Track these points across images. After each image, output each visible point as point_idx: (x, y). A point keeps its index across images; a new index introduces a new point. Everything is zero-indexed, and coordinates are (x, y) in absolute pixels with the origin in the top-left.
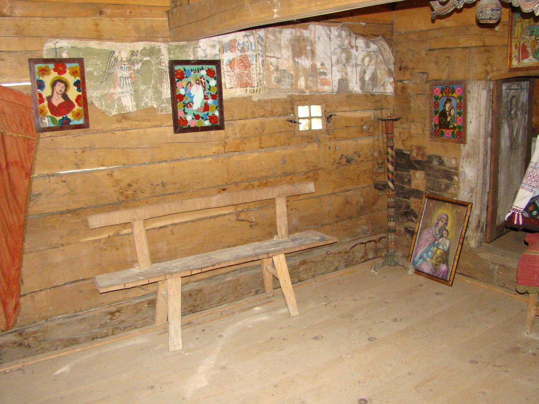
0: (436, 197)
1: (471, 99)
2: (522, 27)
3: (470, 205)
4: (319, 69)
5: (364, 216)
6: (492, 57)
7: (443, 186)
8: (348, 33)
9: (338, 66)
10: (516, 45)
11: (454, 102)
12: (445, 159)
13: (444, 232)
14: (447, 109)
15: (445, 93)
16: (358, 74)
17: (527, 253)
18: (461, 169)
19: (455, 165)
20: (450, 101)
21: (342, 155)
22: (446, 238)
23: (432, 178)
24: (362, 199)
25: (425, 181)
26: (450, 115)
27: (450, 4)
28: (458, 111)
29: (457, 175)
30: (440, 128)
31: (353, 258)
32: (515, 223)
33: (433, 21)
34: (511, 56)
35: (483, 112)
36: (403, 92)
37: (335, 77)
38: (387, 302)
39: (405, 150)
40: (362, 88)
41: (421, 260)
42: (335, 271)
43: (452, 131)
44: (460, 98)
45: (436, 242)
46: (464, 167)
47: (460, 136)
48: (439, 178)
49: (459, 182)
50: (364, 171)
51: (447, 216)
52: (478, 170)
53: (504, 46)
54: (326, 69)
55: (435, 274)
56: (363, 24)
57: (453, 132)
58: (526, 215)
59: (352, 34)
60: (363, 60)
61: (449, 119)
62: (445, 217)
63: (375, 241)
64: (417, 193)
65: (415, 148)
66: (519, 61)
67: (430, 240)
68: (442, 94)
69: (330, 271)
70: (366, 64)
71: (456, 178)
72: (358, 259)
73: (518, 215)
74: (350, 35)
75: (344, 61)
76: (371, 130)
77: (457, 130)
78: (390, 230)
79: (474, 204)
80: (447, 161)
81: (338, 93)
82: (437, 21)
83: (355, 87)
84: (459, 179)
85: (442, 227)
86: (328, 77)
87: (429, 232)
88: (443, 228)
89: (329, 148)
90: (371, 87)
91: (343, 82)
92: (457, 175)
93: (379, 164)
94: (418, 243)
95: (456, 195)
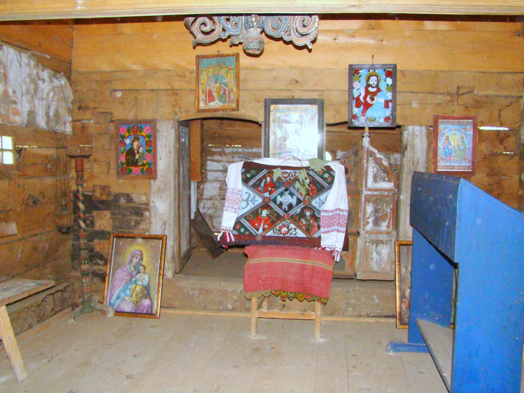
0: (125, 235)
1: (160, 137)
2: (208, 76)
3: (165, 237)
4: (11, 96)
5: (50, 264)
6: (180, 100)
7: (133, 223)
8: (36, 64)
9: (27, 96)
10: (203, 90)
11: (143, 141)
12: (134, 196)
13: (141, 268)
14: (135, 147)
15: (133, 132)
16: (44, 107)
17: (251, 263)
18: (152, 204)
19: (146, 201)
20: (138, 139)
21: (30, 196)
22: (144, 273)
23: (119, 217)
24: (47, 246)
25: (111, 221)
26: (138, 152)
27: (216, 34)
28: (148, 148)
29: (148, 210)
30: (127, 166)
31: (44, 313)
32: (228, 240)
33: (194, 48)
34: (198, 100)
35: (172, 149)
36: (83, 132)
37: (24, 107)
38: (111, 344)
39: (86, 192)
40: (47, 123)
41: (119, 300)
42: (29, 329)
43: (141, 168)
44: (149, 136)
45: (134, 279)
46: (155, 201)
47: (151, 172)
48: (128, 216)
49: (150, 217)
50: (49, 214)
51: (141, 252)
52: (170, 203)
53: (191, 90)
54: (17, 97)
55: (138, 311)
56: (48, 57)
57: (142, 170)
58: (236, 233)
59: (40, 65)
60: (48, 94)
61: (137, 157)
62: (139, 253)
63: (61, 291)
64: (103, 235)
65: (98, 187)
66: (206, 104)
67: (126, 278)
68: (129, 132)
69: (24, 329)
70: (50, 99)
71: (147, 213)
72: (48, 313)
73: (229, 234)
74: (38, 65)
75: (32, 92)
76: (54, 169)
77: (147, 167)
78: (84, 274)
79: (168, 236)
80: (136, 197)
81: (27, 125)
82: (198, 47)
83: (41, 122)
84: (150, 214)
85: (137, 263)
86: (19, 106)
87: (124, 271)
88: (139, 264)
89: (19, 187)
90: (54, 124)
91: (32, 114)
92: (148, 210)
93: (62, 206)
94: (112, 284)
95: (148, 230)
